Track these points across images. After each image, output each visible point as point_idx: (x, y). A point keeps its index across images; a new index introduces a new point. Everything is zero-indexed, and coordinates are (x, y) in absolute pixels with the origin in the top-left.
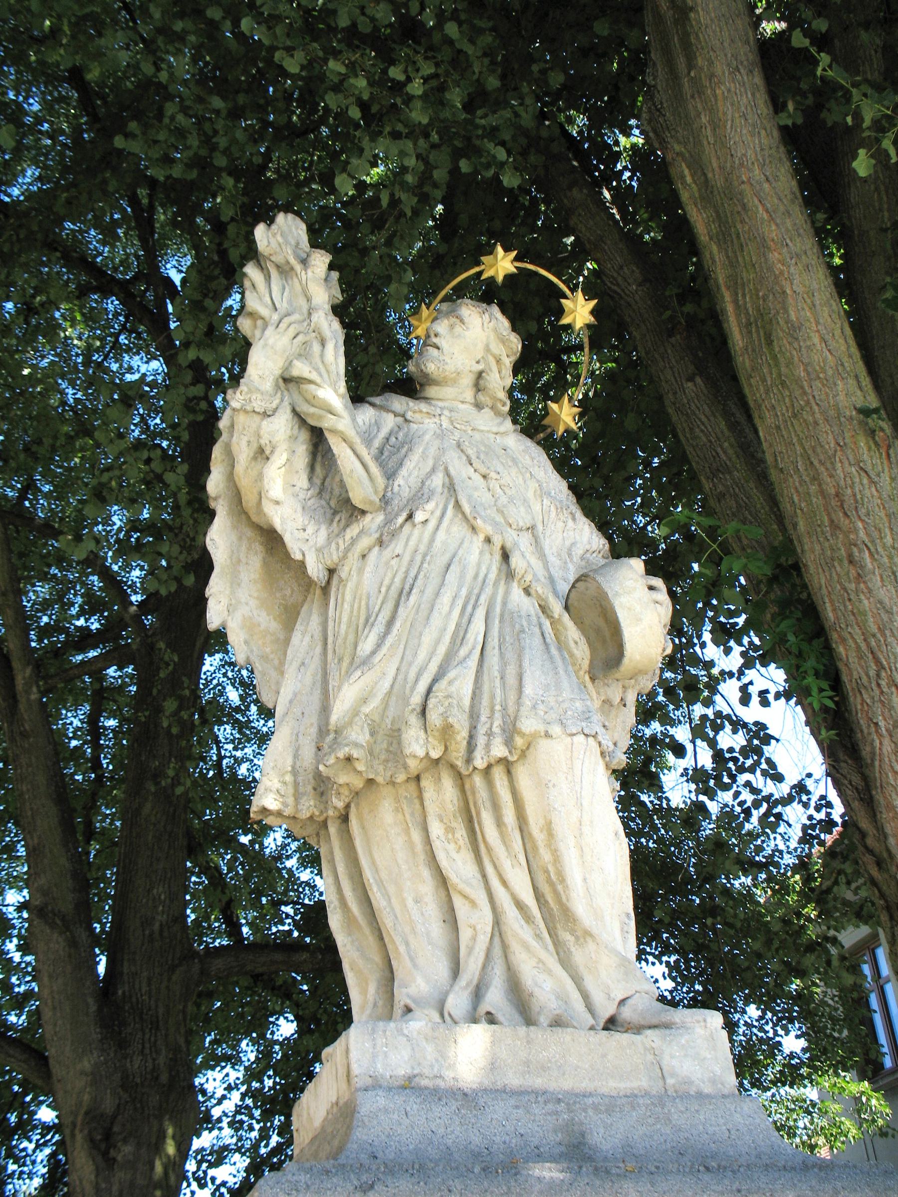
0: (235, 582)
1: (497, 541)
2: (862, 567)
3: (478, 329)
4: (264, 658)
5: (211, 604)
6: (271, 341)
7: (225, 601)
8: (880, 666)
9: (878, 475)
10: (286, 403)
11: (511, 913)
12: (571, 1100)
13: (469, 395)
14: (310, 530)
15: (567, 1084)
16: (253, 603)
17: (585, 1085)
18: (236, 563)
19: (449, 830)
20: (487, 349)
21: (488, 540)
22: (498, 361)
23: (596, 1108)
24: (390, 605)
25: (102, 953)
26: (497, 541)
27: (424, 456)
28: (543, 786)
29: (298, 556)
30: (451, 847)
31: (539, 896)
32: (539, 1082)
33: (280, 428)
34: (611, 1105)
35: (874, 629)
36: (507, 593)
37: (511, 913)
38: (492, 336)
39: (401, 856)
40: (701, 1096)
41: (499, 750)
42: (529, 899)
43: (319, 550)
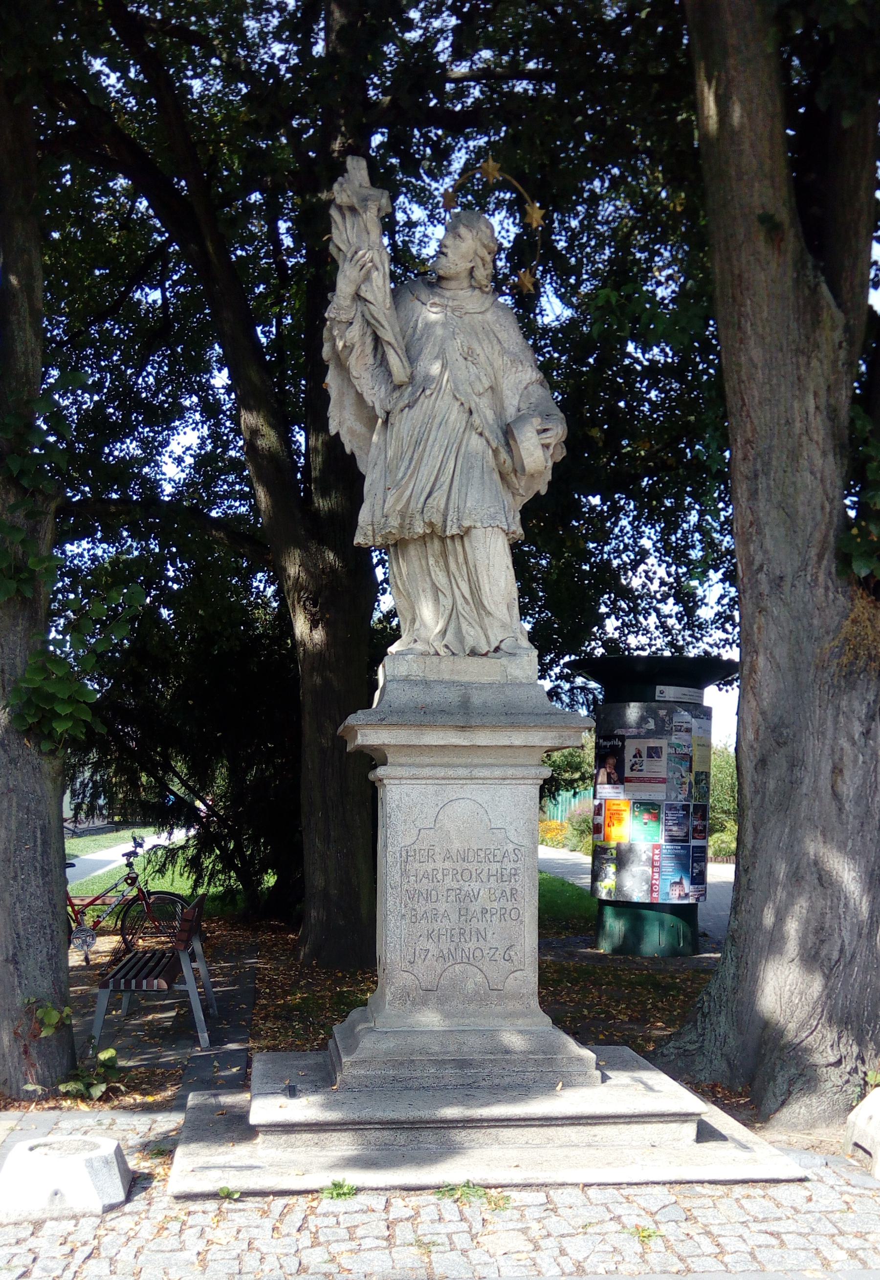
0: (342, 407)
1: (466, 406)
2: (745, 333)
3: (470, 241)
4: (361, 448)
5: (330, 421)
6: (348, 273)
7: (337, 421)
8: (744, 404)
9: (768, 263)
10: (359, 314)
11: (460, 601)
12: (466, 685)
13: (465, 284)
14: (376, 389)
15: (466, 679)
16: (352, 418)
17: (474, 679)
18: (341, 394)
19: (437, 562)
20: (476, 253)
21: (462, 404)
22: (482, 259)
23: (476, 688)
24: (411, 449)
25: (334, 151)
26: (466, 406)
27: (434, 345)
28: (474, 549)
29: (371, 404)
30: (437, 569)
31: (472, 593)
32: (456, 678)
33: (354, 333)
34: (482, 687)
35: (745, 378)
36: (469, 438)
37: (460, 601)
38: (479, 244)
39: (417, 570)
40: (521, 684)
41: (455, 531)
42: (468, 595)
43: (381, 401)
